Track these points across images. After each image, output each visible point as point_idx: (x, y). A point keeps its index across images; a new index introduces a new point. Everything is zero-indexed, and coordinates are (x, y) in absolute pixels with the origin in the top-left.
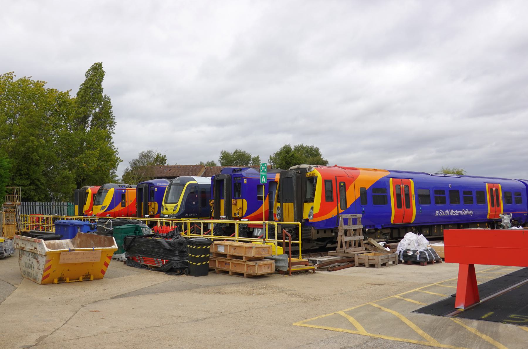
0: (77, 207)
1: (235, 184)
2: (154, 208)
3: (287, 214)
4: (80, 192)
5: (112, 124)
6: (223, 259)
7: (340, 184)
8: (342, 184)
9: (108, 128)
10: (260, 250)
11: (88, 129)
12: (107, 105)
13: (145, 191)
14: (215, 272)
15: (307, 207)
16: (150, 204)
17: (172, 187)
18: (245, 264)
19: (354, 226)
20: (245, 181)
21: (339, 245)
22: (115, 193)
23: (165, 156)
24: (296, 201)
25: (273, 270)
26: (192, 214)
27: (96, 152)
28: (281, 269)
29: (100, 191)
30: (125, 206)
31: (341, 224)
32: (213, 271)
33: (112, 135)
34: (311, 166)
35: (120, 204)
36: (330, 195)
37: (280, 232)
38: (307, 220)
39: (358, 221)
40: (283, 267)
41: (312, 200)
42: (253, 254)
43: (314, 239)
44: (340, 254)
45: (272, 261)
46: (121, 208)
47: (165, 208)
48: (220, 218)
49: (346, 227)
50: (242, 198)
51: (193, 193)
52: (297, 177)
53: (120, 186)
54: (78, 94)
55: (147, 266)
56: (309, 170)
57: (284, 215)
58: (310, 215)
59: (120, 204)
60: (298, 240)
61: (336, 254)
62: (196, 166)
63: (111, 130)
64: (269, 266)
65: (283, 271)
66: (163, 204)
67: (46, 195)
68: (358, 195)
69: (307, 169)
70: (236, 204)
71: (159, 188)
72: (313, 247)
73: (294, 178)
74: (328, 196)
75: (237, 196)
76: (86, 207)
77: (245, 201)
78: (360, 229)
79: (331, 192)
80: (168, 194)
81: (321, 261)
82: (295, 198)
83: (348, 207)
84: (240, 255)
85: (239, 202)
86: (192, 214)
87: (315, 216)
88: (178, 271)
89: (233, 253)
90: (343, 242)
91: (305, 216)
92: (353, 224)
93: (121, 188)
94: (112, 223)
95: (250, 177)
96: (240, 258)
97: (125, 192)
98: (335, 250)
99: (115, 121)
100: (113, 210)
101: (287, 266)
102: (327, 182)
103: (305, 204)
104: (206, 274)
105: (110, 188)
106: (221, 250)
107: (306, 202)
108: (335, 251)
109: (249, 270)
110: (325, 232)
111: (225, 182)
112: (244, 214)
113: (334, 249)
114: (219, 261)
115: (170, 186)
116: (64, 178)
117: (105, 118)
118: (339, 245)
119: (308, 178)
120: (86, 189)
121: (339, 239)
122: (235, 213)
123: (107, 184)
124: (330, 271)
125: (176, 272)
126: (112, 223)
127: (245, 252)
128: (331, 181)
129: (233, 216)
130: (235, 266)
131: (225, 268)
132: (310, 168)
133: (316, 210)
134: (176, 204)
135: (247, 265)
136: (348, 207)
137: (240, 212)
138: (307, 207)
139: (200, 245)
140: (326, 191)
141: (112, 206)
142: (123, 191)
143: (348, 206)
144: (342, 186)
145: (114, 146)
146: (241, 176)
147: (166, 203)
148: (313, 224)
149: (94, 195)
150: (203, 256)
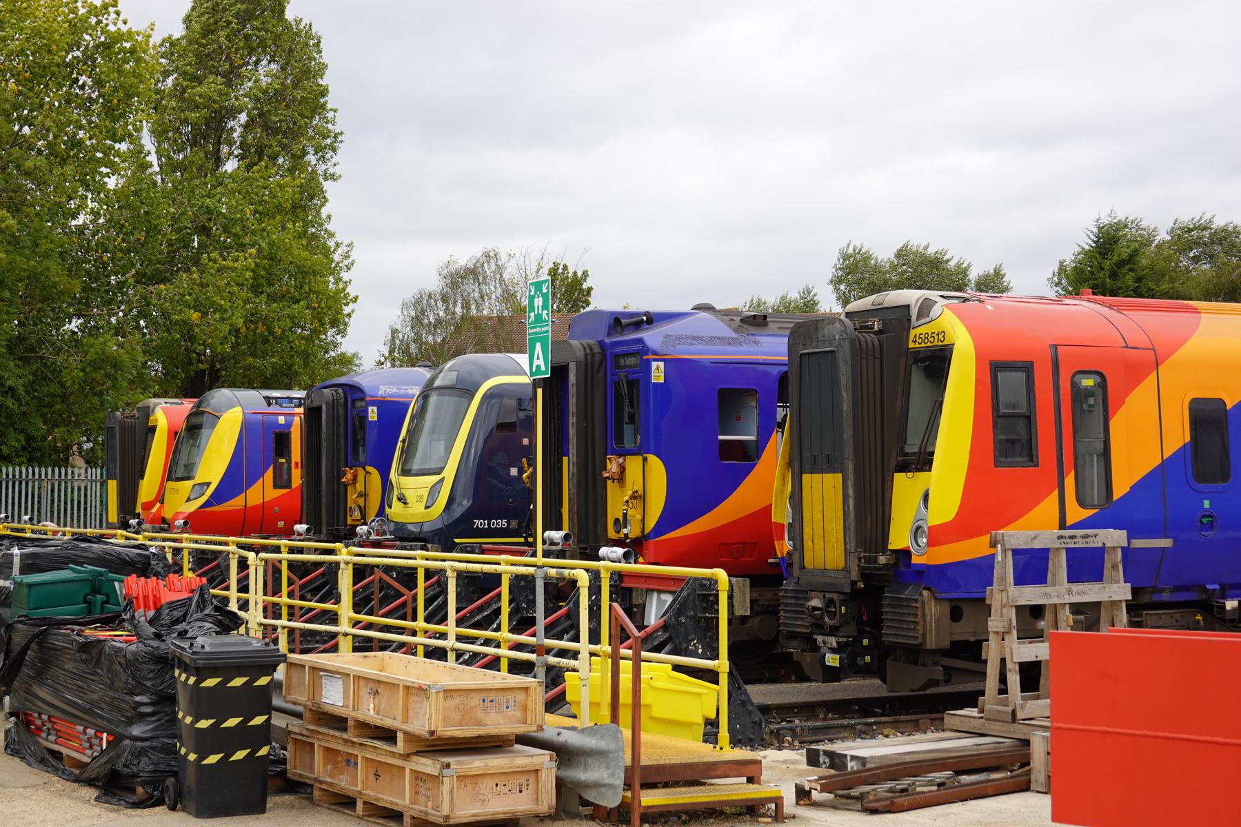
0: (113, 485)
1: (617, 384)
2: (364, 495)
3: (818, 525)
4: (123, 427)
5: (327, 144)
6: (332, 738)
7: (1074, 385)
8: (1088, 382)
9: (311, 158)
10: (476, 700)
11: (230, 166)
12: (298, 54)
13: (333, 418)
14: (310, 799)
15: (905, 487)
16: (612, 466)
17: (433, 399)
18: (408, 766)
19: (1076, 587)
20: (658, 373)
21: (992, 683)
22: (247, 429)
23: (585, 274)
24: (850, 467)
25: (547, 800)
26: (502, 523)
27: (245, 261)
28: (591, 796)
29: (195, 420)
30: (288, 485)
31: (1003, 579)
32: (296, 787)
33: (327, 185)
34: (933, 294)
35: (269, 474)
36: (1024, 436)
37: (743, 610)
38: (906, 553)
39: (1108, 565)
40: (596, 785)
41: (924, 462)
42: (428, 719)
43: (931, 644)
44: (996, 727)
45: (543, 758)
46: (273, 494)
47: (396, 493)
48: (293, 533)
49: (1030, 595)
50: (640, 451)
51: (510, 426)
52: (859, 351)
53: (267, 399)
54: (188, 20)
55: (57, 755)
56: (920, 315)
57: (807, 530)
58: (917, 531)
59: (269, 474)
60: (715, 656)
61: (977, 725)
62: (970, 332)
63: (321, 168)
64: (522, 779)
65: (597, 807)
66: (393, 475)
67: (30, 438)
68: (1178, 435)
69: (914, 313)
70: (621, 478)
71: (383, 405)
72: (935, 683)
73: (844, 355)
74: (1009, 436)
75: (628, 444)
76: (147, 489)
77: (655, 463)
78: (1114, 604)
79: (1028, 419)
80: (414, 433)
81: (863, 761)
82: (849, 452)
83: (1116, 496)
84: (388, 723)
85: (633, 464)
86: (502, 523)
87: (939, 535)
88: (140, 790)
89: (369, 711)
90: (1009, 665)
91: (899, 538)
92: (1072, 579)
93: (275, 409)
94: (17, 562)
95: (683, 352)
96: (389, 736)
97: (289, 425)
98: (974, 704)
99: (337, 128)
100: (237, 503)
101: (619, 780)
102: (995, 370)
103: (899, 478)
104: (258, 808)
105: (231, 406)
106: (333, 696)
107: (903, 468)
108: (973, 712)
109: (422, 799)
110: (151, 622)
111: (572, 378)
112: (651, 523)
113: (971, 699)
114: (328, 750)
115: (425, 397)
116: (96, 366)
117: (294, 119)
118: (992, 683)
119: (916, 352)
120: (147, 412)
121: (992, 652)
122: (617, 520)
123: (226, 392)
124: (874, 812)
125: (133, 791)
126: (17, 562)
127: (406, 709)
128: (1027, 368)
129: (612, 534)
130: (377, 776)
131: (343, 783)
132: (926, 306)
133: (944, 509)
134: (434, 479)
135: (418, 776)
136: (1116, 496)
137: (635, 514)
138: (905, 487)
139: (213, 671)
140: (998, 416)
141: (233, 482)
142: (282, 420)
143: (1120, 488)
144: (1088, 393)
145: (331, 235)
146: (642, 350)
147: (406, 472)
148: (925, 575)
149: (173, 434)
150: (232, 722)
